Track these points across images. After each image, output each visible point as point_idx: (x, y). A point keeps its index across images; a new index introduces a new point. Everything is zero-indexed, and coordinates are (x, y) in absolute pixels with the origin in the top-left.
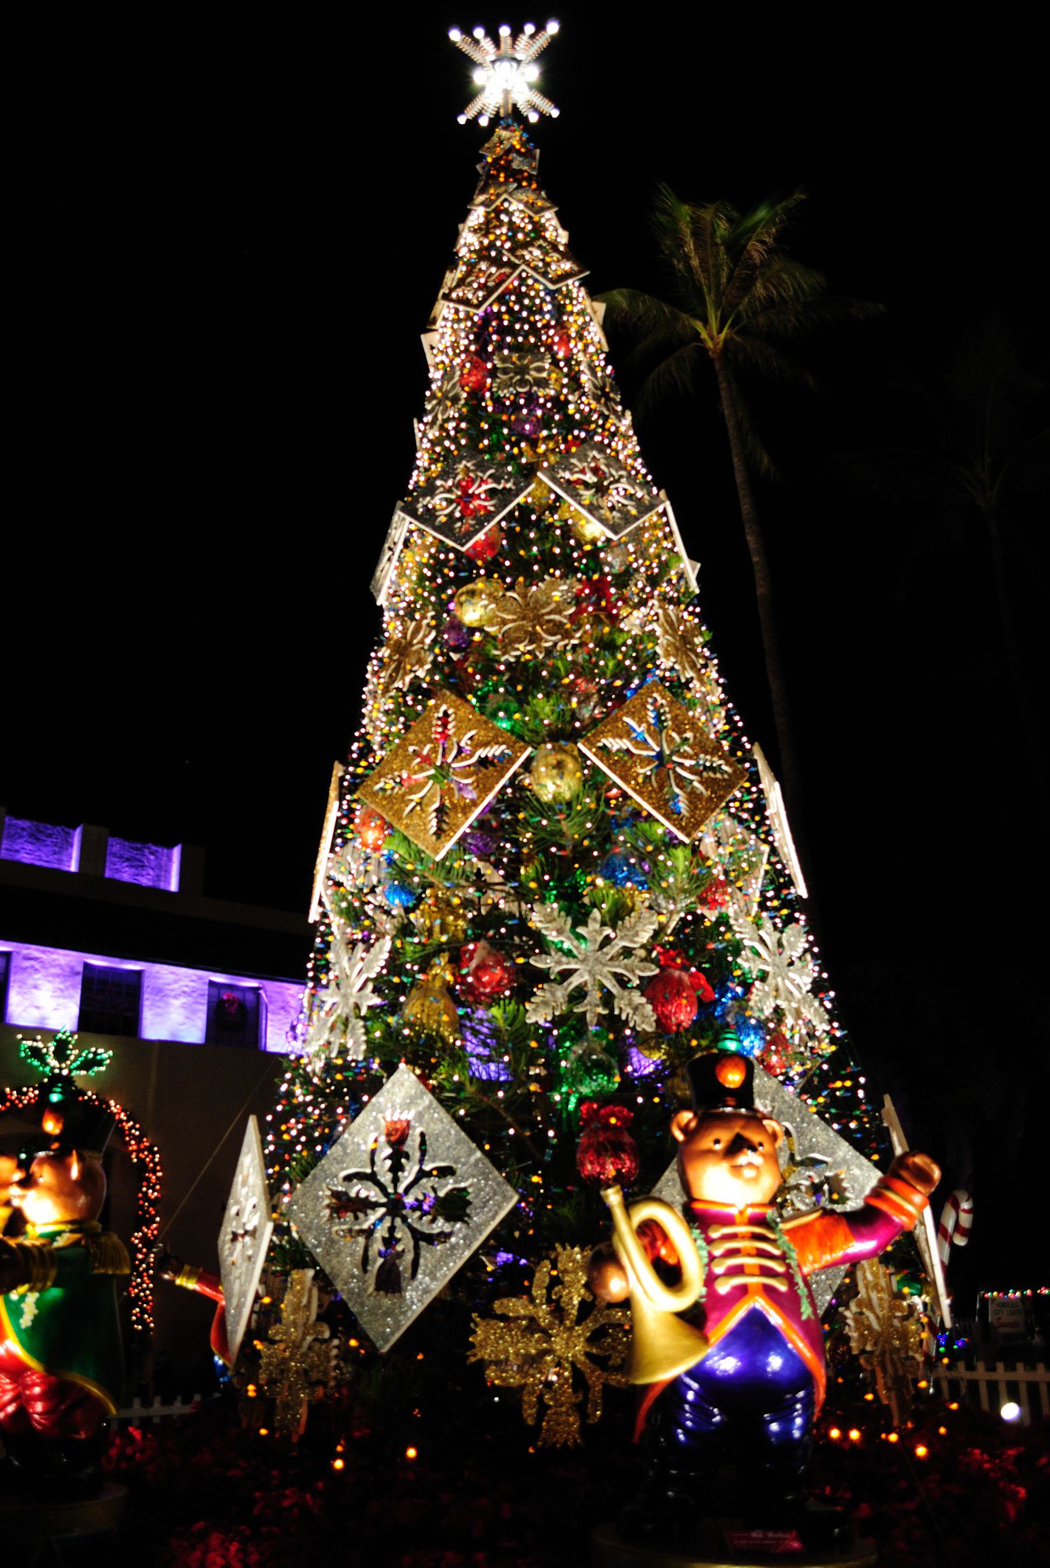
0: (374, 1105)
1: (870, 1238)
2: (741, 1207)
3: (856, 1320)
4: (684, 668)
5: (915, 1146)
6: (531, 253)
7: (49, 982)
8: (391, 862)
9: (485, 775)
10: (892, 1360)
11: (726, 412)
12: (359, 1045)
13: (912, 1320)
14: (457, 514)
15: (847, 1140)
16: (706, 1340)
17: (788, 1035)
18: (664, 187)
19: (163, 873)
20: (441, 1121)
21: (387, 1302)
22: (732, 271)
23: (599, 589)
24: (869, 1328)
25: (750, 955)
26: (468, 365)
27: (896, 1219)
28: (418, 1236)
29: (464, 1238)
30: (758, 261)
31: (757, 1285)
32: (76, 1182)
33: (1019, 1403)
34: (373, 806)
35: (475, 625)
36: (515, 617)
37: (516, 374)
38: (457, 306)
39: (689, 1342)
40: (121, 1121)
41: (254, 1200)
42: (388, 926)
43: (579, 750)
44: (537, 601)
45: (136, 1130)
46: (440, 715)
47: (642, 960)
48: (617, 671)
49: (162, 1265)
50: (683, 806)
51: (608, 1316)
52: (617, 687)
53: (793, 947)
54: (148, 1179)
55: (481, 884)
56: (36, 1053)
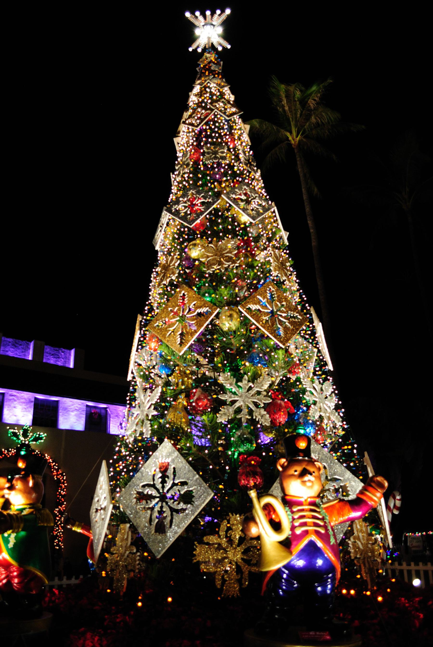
0: (154, 456)
1: (359, 511)
2: (306, 498)
3: (353, 545)
4: (282, 276)
5: (377, 473)
6: (219, 104)
7: (20, 405)
8: (161, 356)
9: (200, 320)
10: (368, 561)
11: (300, 170)
12: (148, 431)
13: (376, 545)
14: (189, 212)
15: (349, 470)
16: (291, 553)
17: (325, 427)
18: (274, 77)
19: (67, 360)
20: (182, 462)
21: (159, 537)
22: (302, 112)
23: (247, 243)
24: (359, 548)
25: (309, 394)
26: (193, 151)
27: (369, 503)
28: (172, 510)
29: (192, 511)
30: (312, 108)
31: (312, 530)
32: (31, 488)
33: (420, 579)
34: (154, 333)
35: (196, 258)
36: (212, 255)
37: (213, 154)
38: (188, 126)
39: (284, 554)
40: (50, 463)
41: (105, 495)
42: (160, 382)
43: (239, 310)
44: (221, 248)
45: (56, 466)
46: (182, 295)
47: (265, 396)
48: (255, 277)
49: (67, 522)
50: (282, 332)
51: (251, 543)
52: (254, 284)
53: (327, 391)
54: (61, 487)
55: (198, 365)
56: (15, 434)
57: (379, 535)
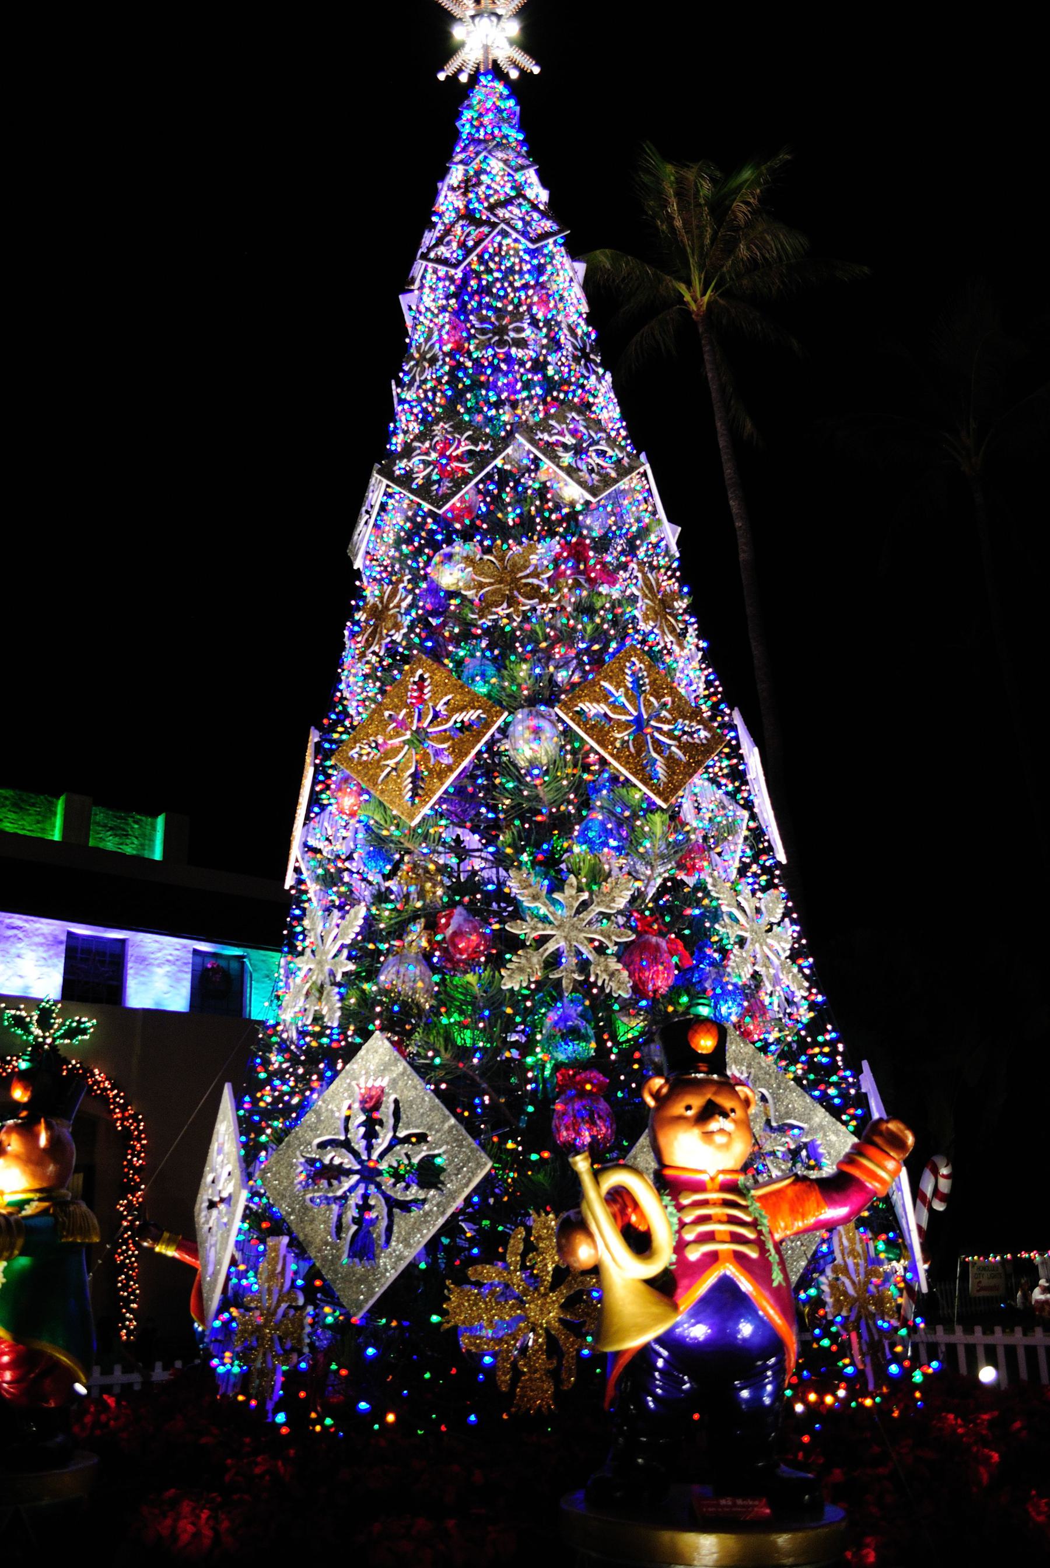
0: (348, 1072)
2: (712, 1173)
4: (663, 632)
5: (893, 1110)
7: (33, 951)
10: (867, 1324)
11: (710, 375)
12: (335, 1012)
16: (675, 1307)
18: (649, 147)
19: (147, 842)
21: (360, 1269)
22: (715, 233)
23: (577, 553)
24: (845, 1293)
27: (868, 1185)
28: (392, 1203)
29: (438, 1205)
31: (727, 1251)
32: (44, 1150)
33: (996, 1366)
34: (348, 772)
35: (452, 588)
36: (492, 581)
37: (495, 334)
38: (436, 266)
39: (657, 1309)
40: (105, 1089)
41: (229, 1168)
43: (557, 715)
44: (514, 565)
45: (121, 1098)
46: (416, 679)
48: (596, 634)
49: (142, 1232)
51: (582, 1282)
52: (595, 651)
53: (771, 913)
54: (133, 1147)
55: (459, 849)
56: (19, 1021)
57: (898, 1261)
